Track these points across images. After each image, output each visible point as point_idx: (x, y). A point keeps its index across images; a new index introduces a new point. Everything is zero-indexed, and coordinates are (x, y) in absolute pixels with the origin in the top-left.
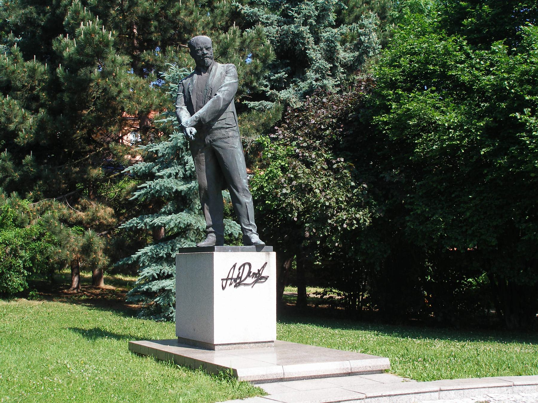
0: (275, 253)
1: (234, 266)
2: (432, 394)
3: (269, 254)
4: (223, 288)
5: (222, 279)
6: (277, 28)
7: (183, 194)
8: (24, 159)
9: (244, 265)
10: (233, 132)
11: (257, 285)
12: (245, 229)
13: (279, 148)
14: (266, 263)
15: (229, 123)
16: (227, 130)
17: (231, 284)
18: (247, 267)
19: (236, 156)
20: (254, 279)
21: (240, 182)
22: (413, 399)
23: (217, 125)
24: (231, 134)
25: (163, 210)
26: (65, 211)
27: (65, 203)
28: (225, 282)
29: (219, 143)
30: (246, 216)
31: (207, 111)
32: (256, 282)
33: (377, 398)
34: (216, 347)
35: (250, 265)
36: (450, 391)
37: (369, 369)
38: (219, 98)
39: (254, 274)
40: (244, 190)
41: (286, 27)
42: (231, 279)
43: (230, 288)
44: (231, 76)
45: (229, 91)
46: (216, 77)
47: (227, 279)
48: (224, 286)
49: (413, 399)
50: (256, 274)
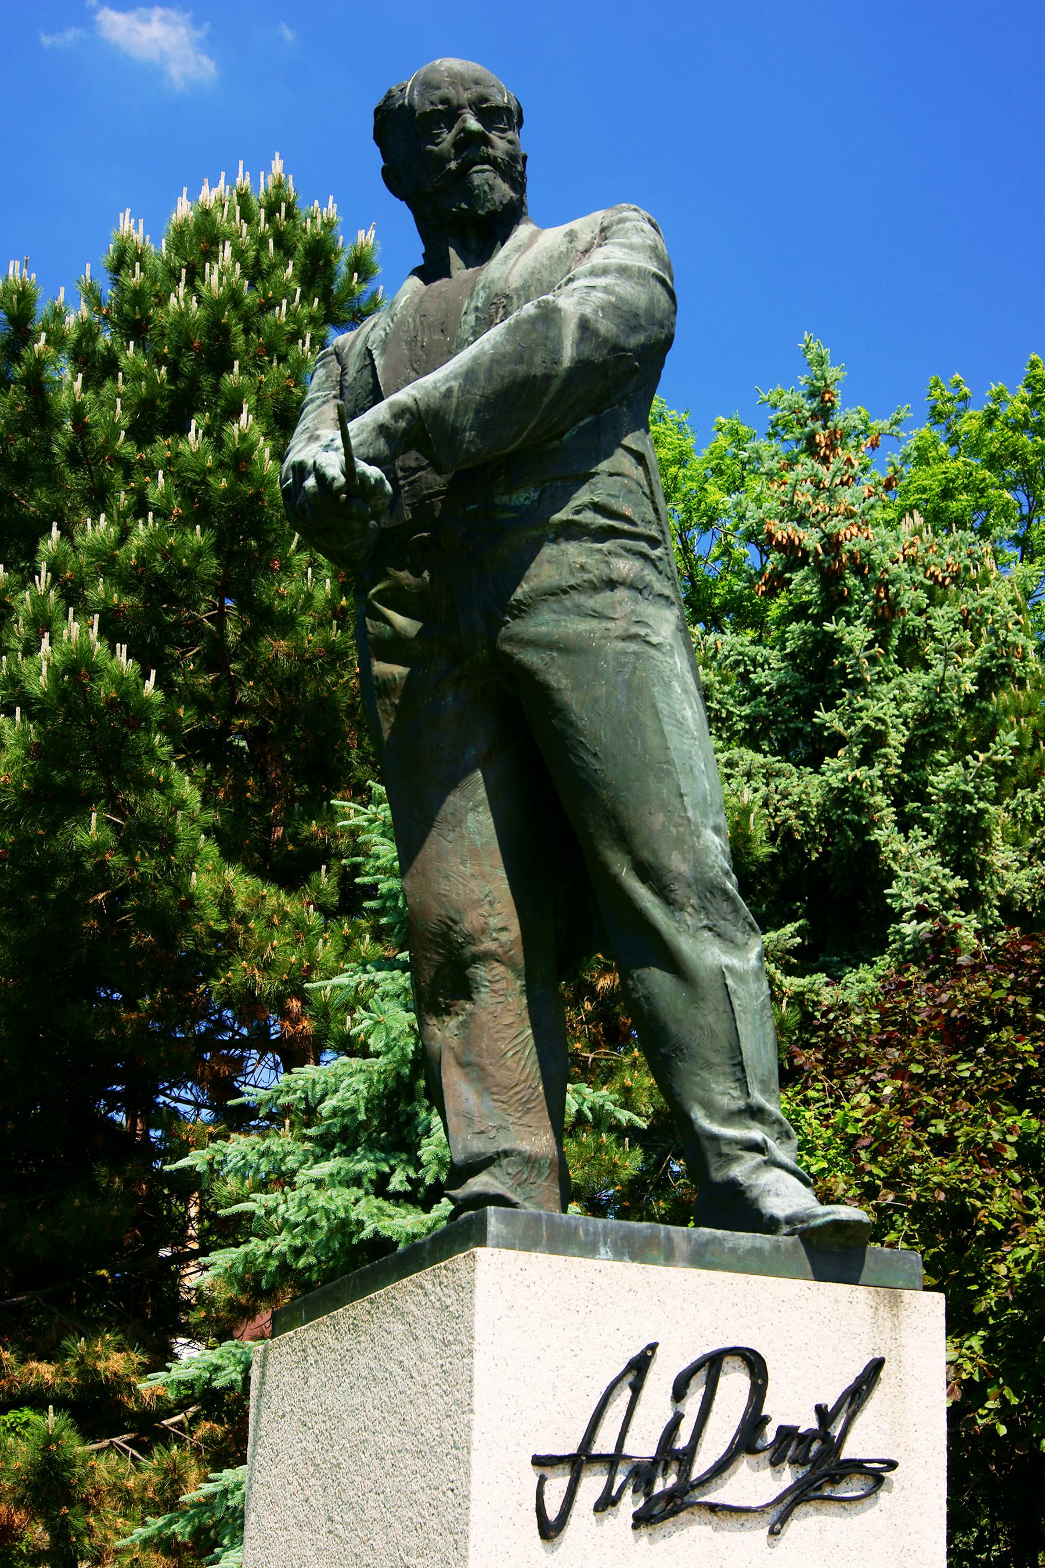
0: (938, 1300)
1: (639, 1366)
3: (895, 1303)
4: (550, 1530)
9: (712, 1365)
11: (809, 1525)
12: (715, 1138)
14: (876, 1367)
16: (606, 546)
17: (607, 1502)
18: (734, 1385)
20: (788, 1476)
21: (679, 842)
31: (469, 375)
32: (799, 1496)
35: (755, 1364)
39: (786, 1433)
42: (612, 1461)
45: (620, 299)
47: (578, 1462)
48: (552, 1512)
50: (807, 1438)
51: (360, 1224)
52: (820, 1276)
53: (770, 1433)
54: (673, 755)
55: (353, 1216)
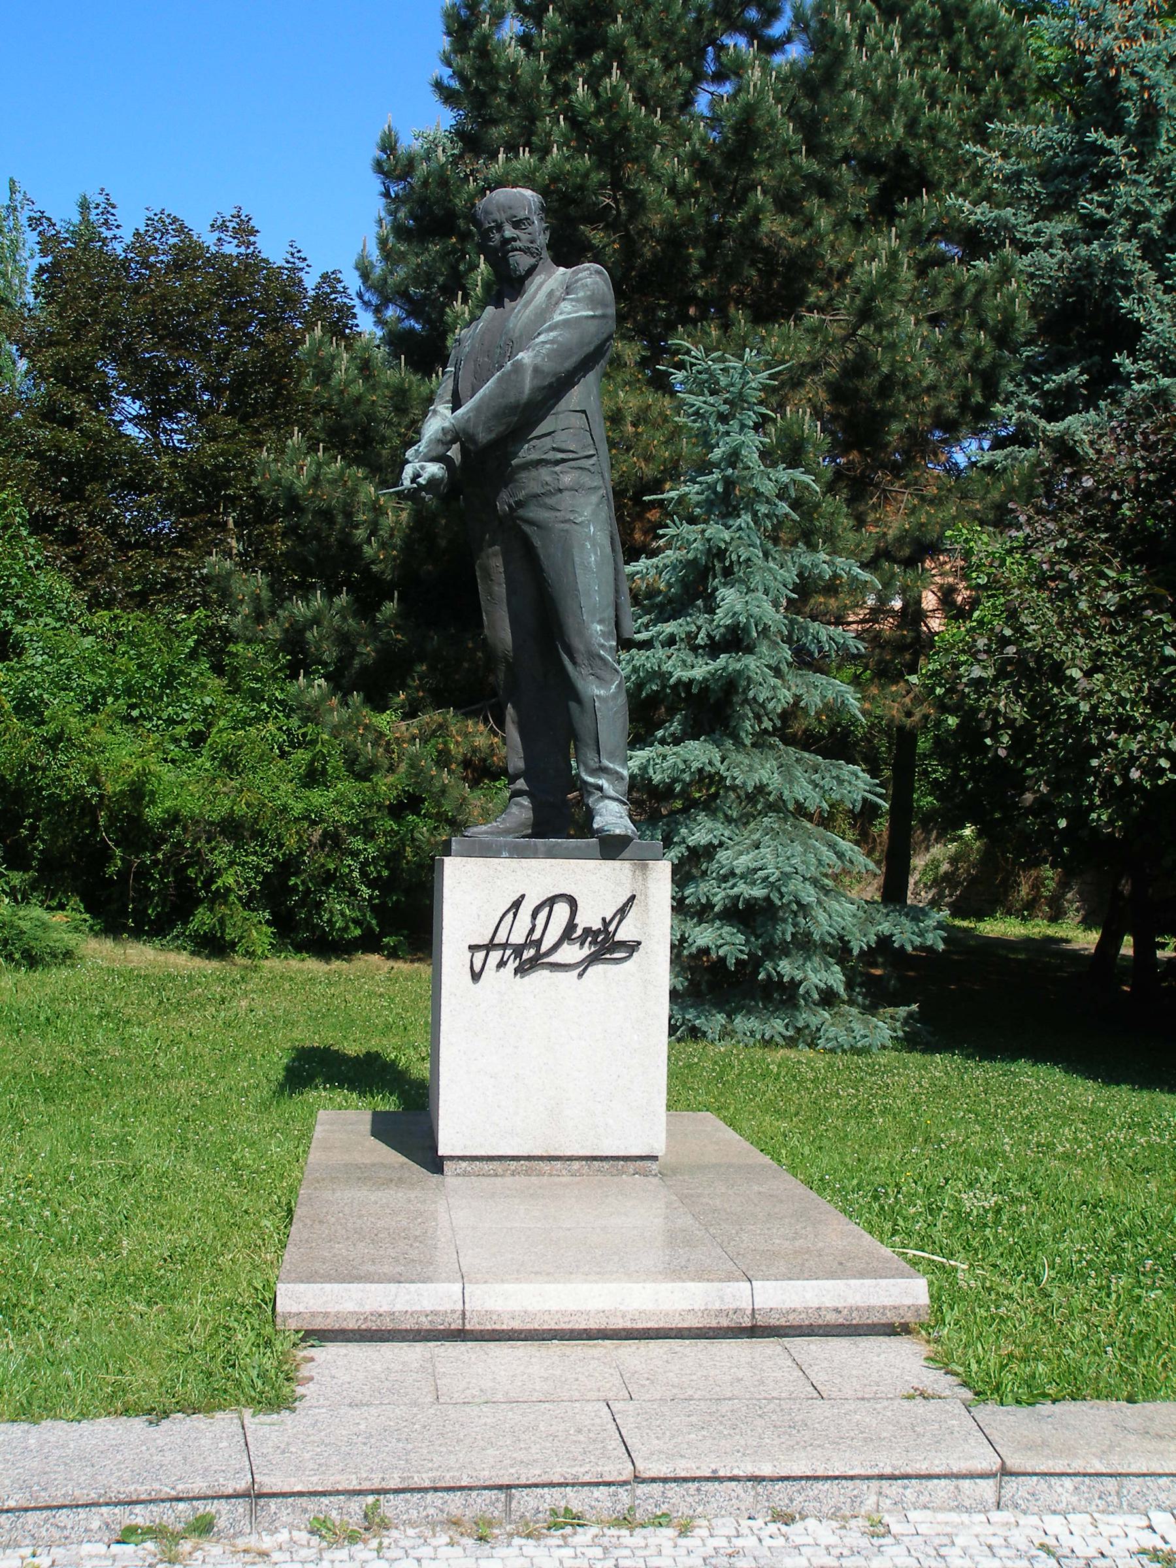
1: (517, 905)
2: (966, 1484)
3: (645, 868)
4: (476, 976)
5: (470, 947)
6: (1060, 254)
7: (695, 690)
8: (379, 610)
9: (551, 901)
10: (577, 473)
11: (596, 970)
13: (1009, 560)
14: (633, 897)
15: (564, 446)
16: (557, 469)
17: (502, 964)
18: (562, 911)
19: (576, 551)
20: (587, 951)
22: (871, 1501)
23: (527, 453)
24: (567, 479)
25: (660, 733)
26: (480, 741)
27: (486, 721)
28: (480, 955)
29: (534, 512)
30: (591, 742)
32: (592, 959)
33: (693, 1486)
34: (448, 1166)
36: (1053, 1480)
37: (831, 1318)
38: (518, 367)
39: (587, 931)
40: (594, 656)
41: (1083, 250)
42: (504, 946)
43: (500, 979)
44: (577, 300)
46: (531, 307)
47: (490, 947)
48: (477, 969)
49: (871, 1501)
51: (671, 673)
52: (605, 857)
53: (579, 932)
54: (580, 586)
55: (664, 668)
